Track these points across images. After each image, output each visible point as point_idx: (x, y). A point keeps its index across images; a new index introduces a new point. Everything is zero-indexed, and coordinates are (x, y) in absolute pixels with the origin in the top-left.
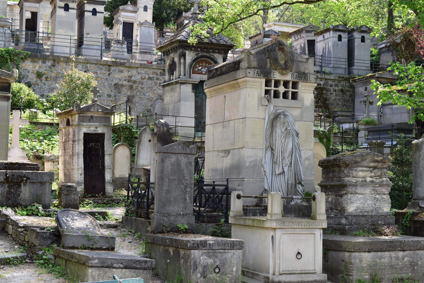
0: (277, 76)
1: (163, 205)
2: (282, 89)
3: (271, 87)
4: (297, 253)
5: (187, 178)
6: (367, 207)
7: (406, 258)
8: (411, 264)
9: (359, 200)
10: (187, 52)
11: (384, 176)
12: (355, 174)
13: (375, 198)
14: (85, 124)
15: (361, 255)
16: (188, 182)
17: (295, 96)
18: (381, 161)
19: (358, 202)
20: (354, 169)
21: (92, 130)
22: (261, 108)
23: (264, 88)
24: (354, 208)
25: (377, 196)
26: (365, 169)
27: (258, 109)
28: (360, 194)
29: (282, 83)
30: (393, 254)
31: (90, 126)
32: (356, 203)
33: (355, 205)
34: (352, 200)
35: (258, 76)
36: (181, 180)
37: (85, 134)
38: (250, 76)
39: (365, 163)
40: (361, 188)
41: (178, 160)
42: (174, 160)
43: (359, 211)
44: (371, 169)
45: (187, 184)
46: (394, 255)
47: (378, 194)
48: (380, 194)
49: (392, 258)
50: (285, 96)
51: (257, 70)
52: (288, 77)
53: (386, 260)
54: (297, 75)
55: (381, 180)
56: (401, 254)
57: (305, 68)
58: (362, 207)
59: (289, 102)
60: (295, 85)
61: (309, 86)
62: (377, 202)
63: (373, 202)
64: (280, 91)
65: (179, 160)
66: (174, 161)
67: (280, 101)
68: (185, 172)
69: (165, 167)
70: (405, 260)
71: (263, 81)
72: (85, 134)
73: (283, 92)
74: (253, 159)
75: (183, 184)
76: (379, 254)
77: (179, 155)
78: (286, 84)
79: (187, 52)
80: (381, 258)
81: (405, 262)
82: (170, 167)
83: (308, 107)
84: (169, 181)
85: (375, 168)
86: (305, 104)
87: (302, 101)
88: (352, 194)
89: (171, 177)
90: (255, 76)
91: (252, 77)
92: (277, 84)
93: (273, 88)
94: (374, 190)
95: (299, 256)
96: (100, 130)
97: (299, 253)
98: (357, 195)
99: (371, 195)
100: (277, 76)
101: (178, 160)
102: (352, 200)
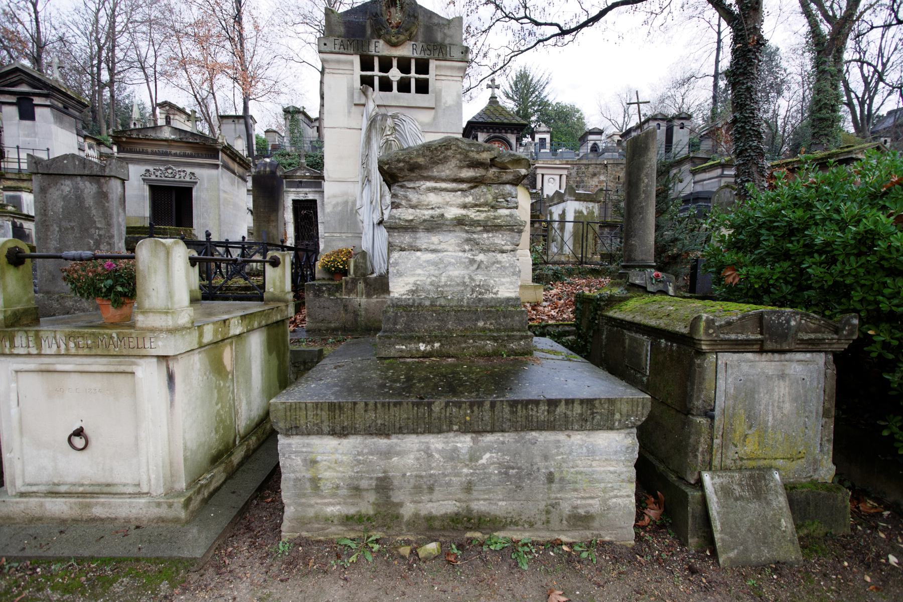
0: (380, 48)
1: (50, 277)
2: (395, 74)
3: (373, 70)
4: (76, 427)
5: (99, 226)
6: (446, 285)
7: (488, 455)
8: (506, 473)
9: (421, 266)
10: (479, 134)
11: (505, 204)
12: (414, 197)
13: (472, 261)
14: (292, 190)
15: (308, 445)
16: (101, 232)
17: (423, 87)
18: (493, 163)
19: (419, 271)
20: (412, 185)
21: (301, 197)
22: (354, 109)
23: (358, 72)
24: (408, 288)
25: (481, 257)
26: (444, 185)
27: (349, 112)
28: (426, 250)
29: (395, 63)
30: (436, 442)
31: (298, 193)
32: (413, 275)
33: (412, 280)
34: (401, 268)
35: (342, 50)
36: (87, 230)
37: (293, 200)
38: (327, 50)
39: (447, 170)
40: (429, 235)
41: (77, 188)
42: (68, 189)
43: (423, 295)
44: (464, 186)
45: (100, 236)
46: (440, 446)
47: (482, 251)
48: (489, 251)
49: (430, 456)
50: (404, 87)
51: (340, 39)
52: (405, 51)
53: (410, 460)
54: (425, 47)
55: (492, 214)
56: (464, 442)
57: (445, 34)
58: (432, 284)
59: (413, 98)
60: (423, 67)
61: (452, 68)
62: (479, 271)
63: (464, 272)
64: (392, 78)
65: (78, 188)
66: (70, 192)
67: (394, 96)
68: (94, 212)
69: (50, 204)
70: (483, 461)
71: (356, 59)
72: (293, 200)
73: (398, 78)
74: (340, 200)
75: (92, 237)
76: (382, 442)
77: (79, 178)
78: (404, 65)
79: (479, 134)
80: (387, 454)
81: (484, 467)
82: (60, 204)
83: (449, 107)
84: (60, 230)
85: (476, 182)
86: (443, 101)
87: (438, 99)
88: (402, 250)
89: (65, 224)
90: (337, 50)
91: (332, 53)
92: (386, 65)
93: (376, 73)
94: (468, 240)
95: (79, 442)
96: (310, 197)
97: (79, 433)
98: (419, 253)
99: (461, 254)
100: (380, 48)
101: (77, 188)
102: (401, 268)
